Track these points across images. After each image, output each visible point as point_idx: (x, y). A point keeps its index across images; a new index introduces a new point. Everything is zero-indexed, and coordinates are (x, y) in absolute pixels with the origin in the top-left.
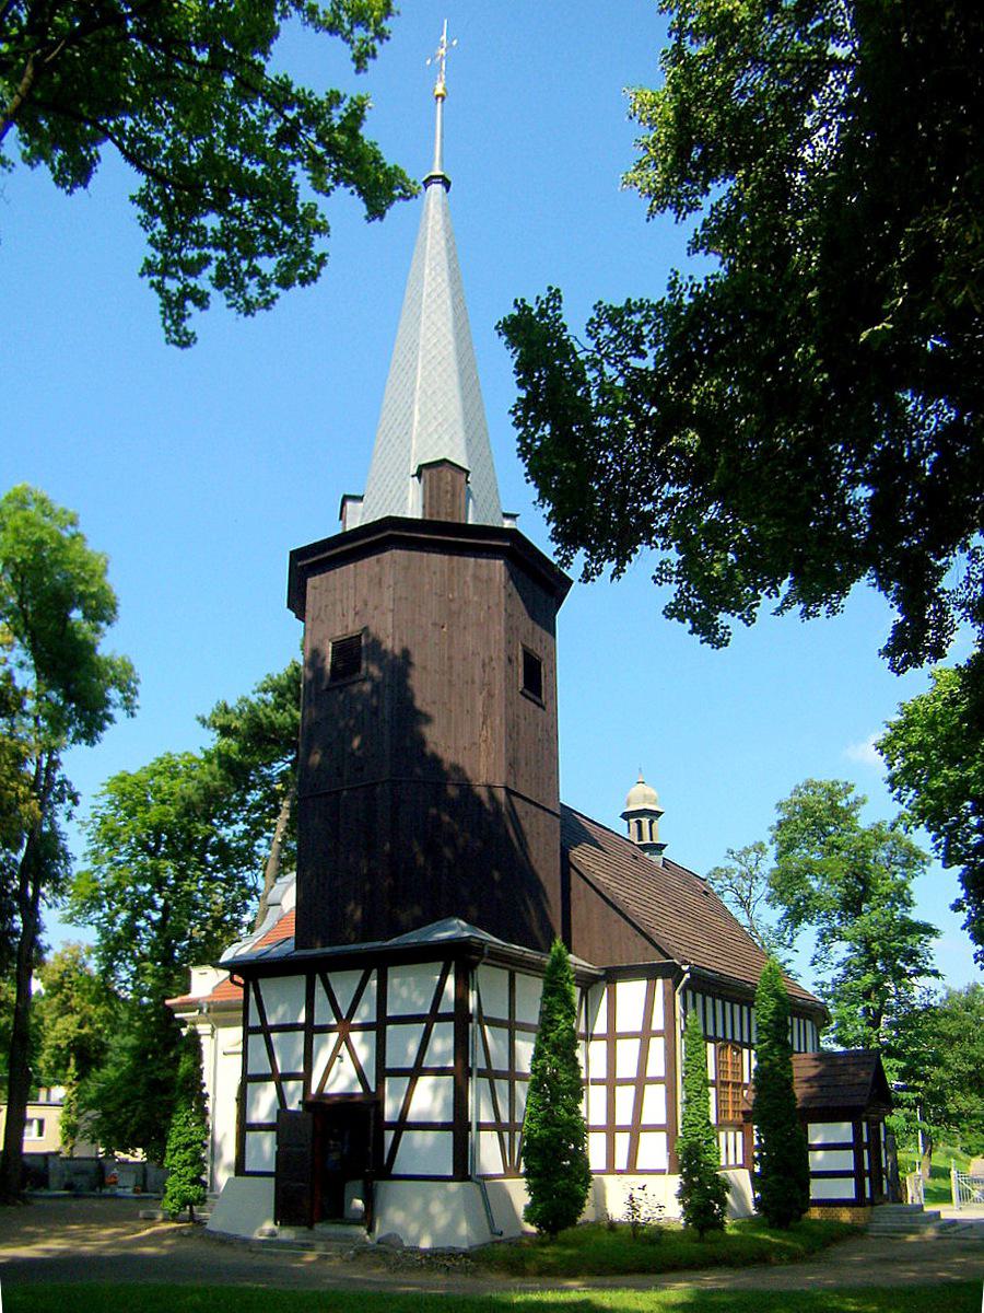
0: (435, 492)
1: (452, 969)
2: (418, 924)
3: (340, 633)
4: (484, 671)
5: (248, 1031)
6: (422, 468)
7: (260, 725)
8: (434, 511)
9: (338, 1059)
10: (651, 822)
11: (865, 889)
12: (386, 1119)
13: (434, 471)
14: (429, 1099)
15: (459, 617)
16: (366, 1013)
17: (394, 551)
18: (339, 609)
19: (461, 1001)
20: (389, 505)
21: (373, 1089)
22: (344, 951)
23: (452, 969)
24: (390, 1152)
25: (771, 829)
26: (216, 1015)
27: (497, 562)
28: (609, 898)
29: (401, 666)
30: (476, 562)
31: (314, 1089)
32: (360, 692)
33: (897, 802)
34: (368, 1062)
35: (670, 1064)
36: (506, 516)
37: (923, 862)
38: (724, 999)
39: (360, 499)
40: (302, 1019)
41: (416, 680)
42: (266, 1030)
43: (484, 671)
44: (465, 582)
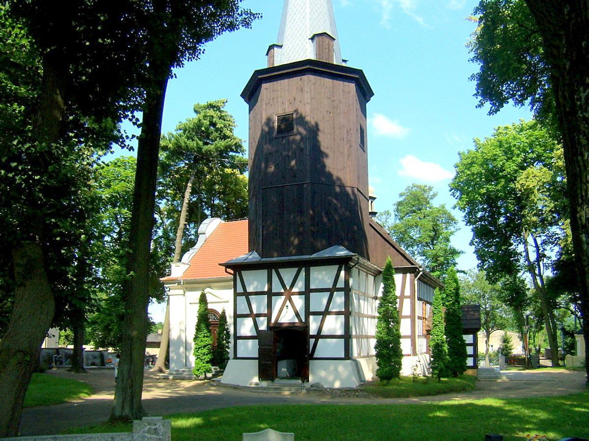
0: (321, 48)
1: (343, 267)
2: (324, 247)
3: (282, 112)
4: (348, 135)
5: (236, 295)
6: (315, 36)
7: (180, 147)
8: (321, 57)
9: (285, 307)
10: (372, 202)
11: (436, 234)
12: (311, 334)
13: (320, 38)
14: (333, 324)
15: (337, 109)
16: (300, 286)
17: (309, 75)
18: (280, 100)
19: (347, 282)
20: (298, 51)
21: (304, 321)
22: (281, 260)
23: (343, 267)
24: (313, 348)
25: (394, 205)
26: (187, 286)
27: (352, 84)
28: (386, 238)
29: (314, 131)
30: (343, 84)
31: (273, 321)
32: (294, 140)
33: (452, 196)
34: (301, 309)
35: (413, 309)
36: (343, 61)
37: (455, 223)
38: (422, 282)
39: (281, 47)
40: (266, 289)
41: (321, 137)
42: (247, 294)
43: (348, 135)
44: (339, 93)
